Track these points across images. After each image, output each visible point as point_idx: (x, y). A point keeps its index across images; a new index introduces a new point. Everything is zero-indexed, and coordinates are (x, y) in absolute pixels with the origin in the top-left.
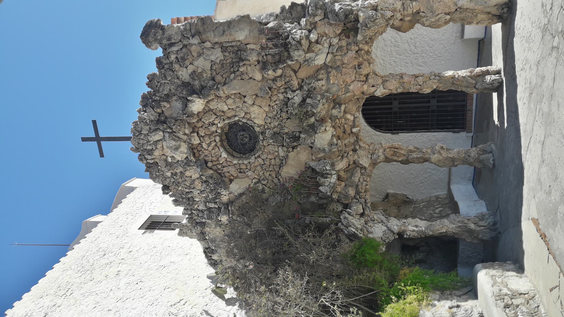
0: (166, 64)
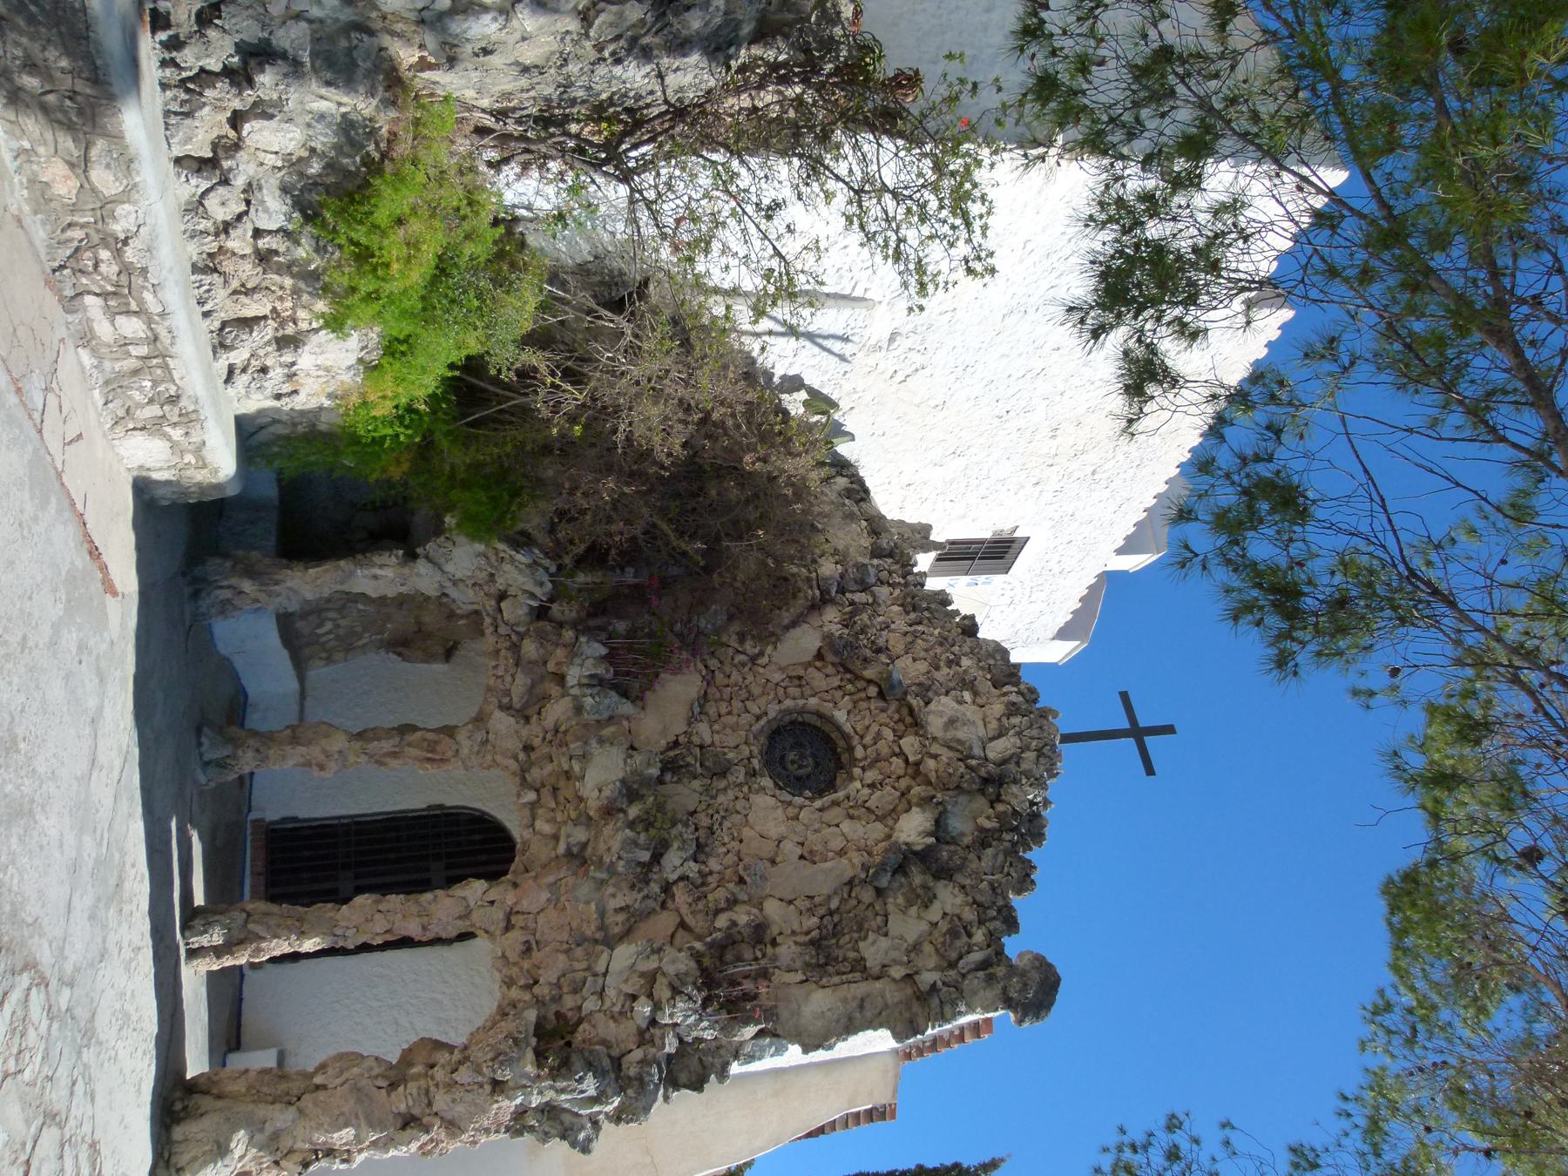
0: (994, 918)
